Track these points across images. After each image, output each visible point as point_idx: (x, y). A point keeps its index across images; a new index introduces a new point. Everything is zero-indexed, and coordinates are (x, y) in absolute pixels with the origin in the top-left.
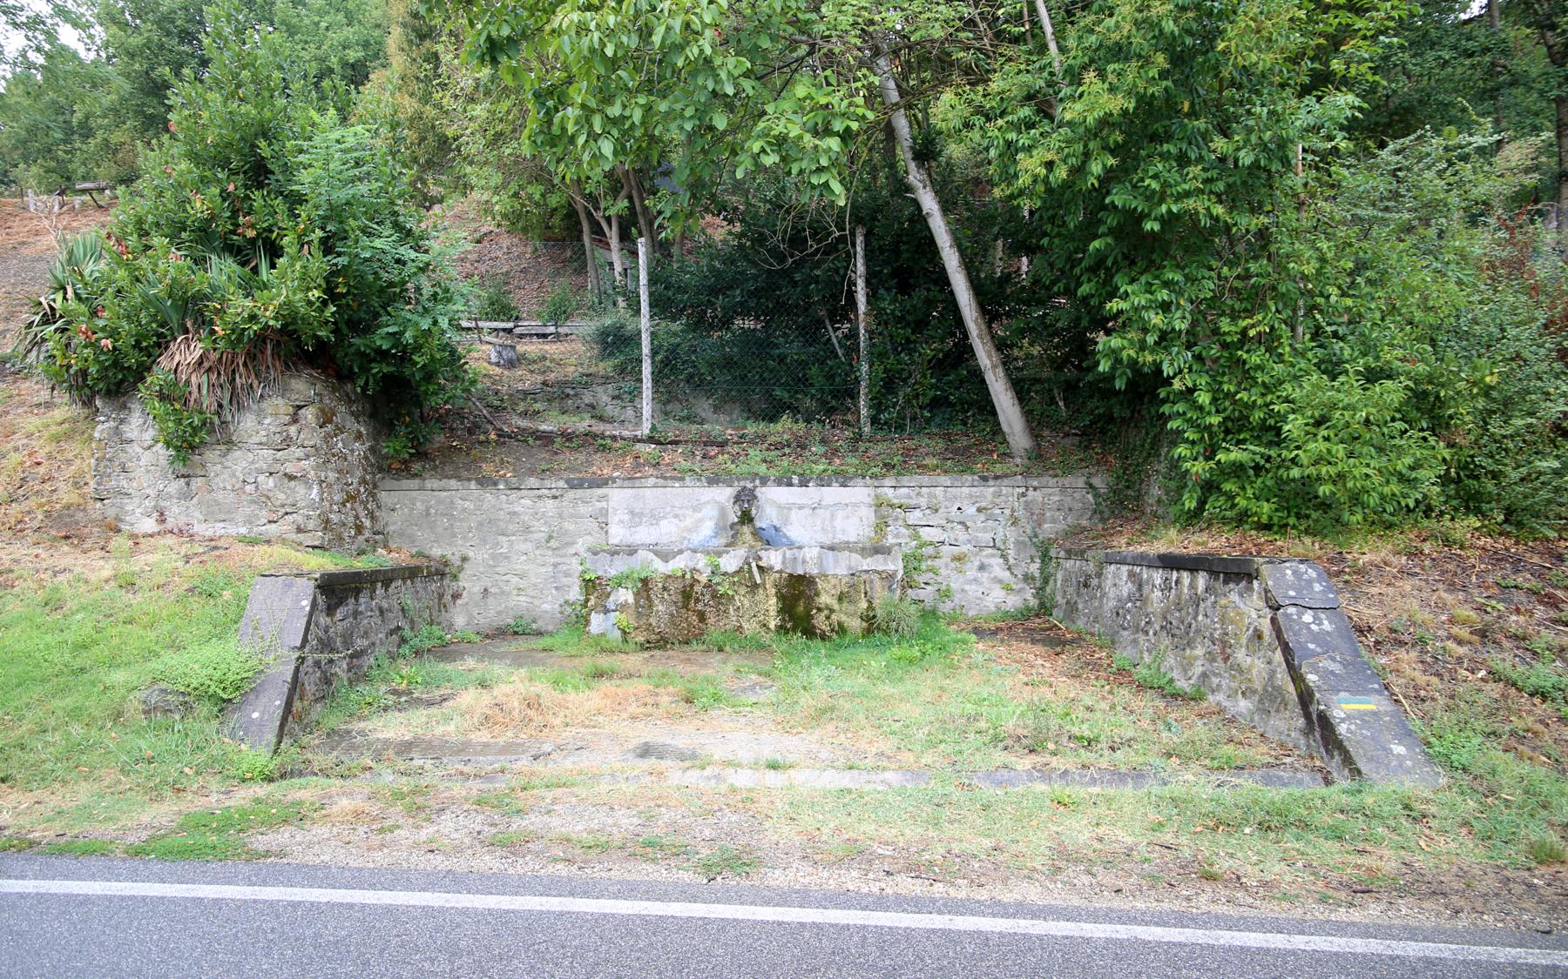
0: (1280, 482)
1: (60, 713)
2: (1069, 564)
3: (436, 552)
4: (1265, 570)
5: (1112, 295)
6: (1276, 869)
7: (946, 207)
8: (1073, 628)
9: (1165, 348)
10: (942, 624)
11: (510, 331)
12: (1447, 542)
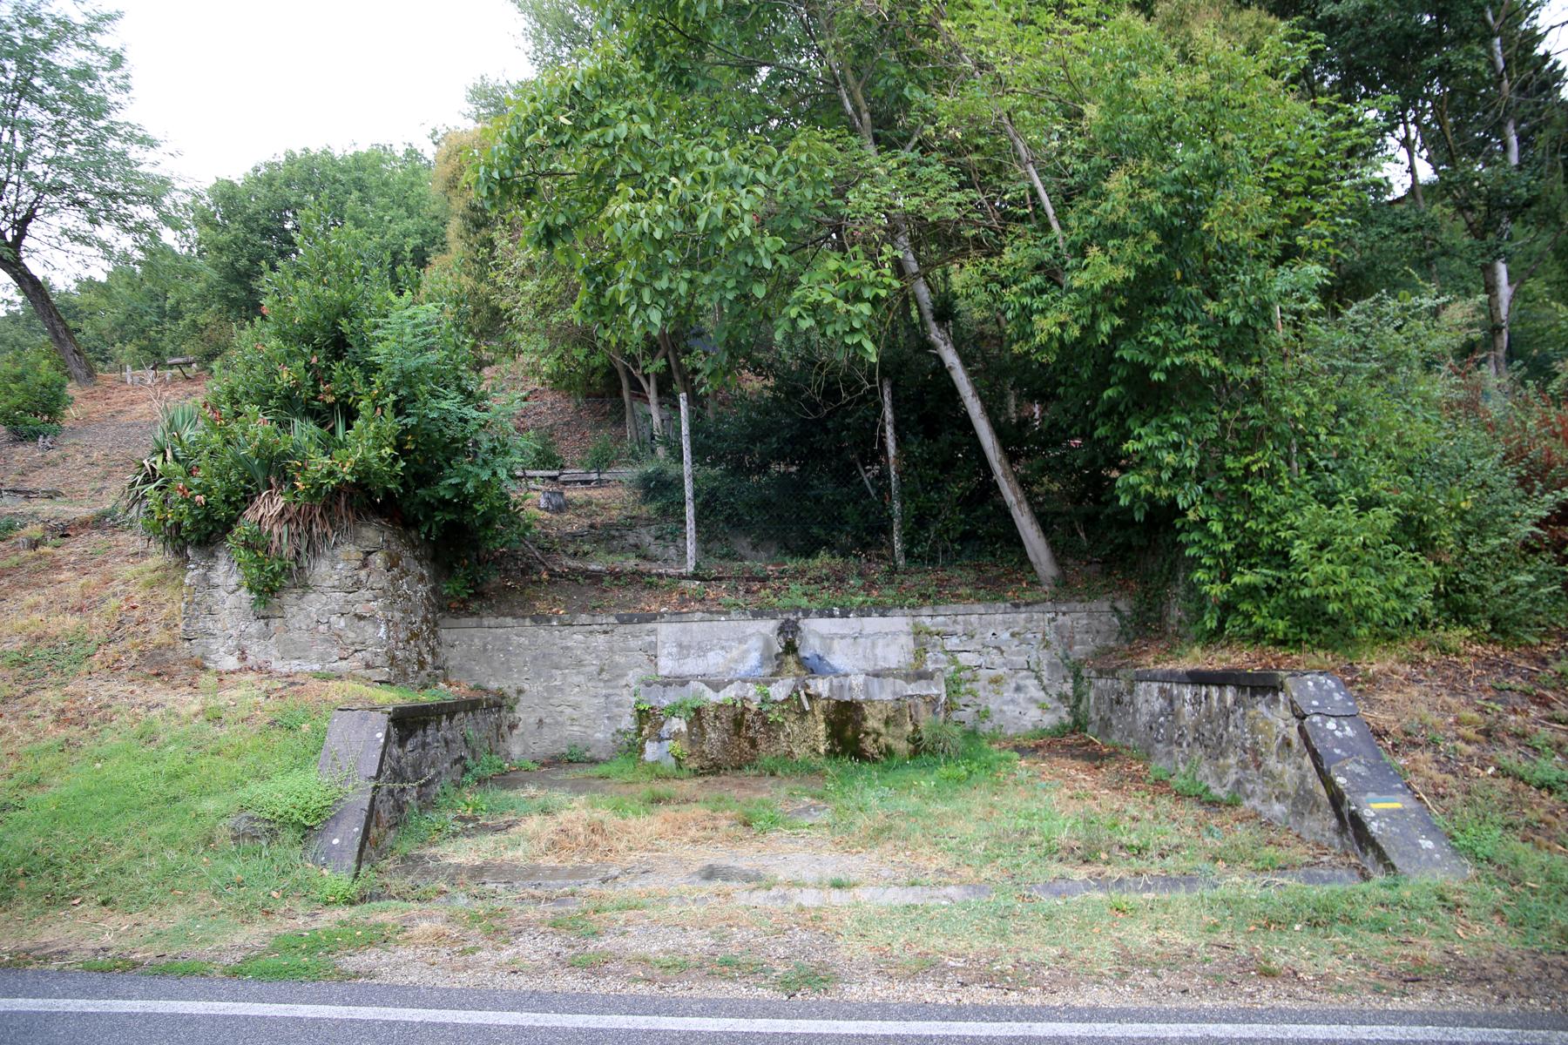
0: (1290, 600)
1: (156, 839)
2: (1100, 683)
3: (493, 685)
4: (1289, 682)
5: (1126, 437)
6: (1329, 963)
7: (966, 361)
8: (1109, 742)
9: (1178, 483)
10: (985, 744)
11: (554, 478)
12: (1445, 650)
